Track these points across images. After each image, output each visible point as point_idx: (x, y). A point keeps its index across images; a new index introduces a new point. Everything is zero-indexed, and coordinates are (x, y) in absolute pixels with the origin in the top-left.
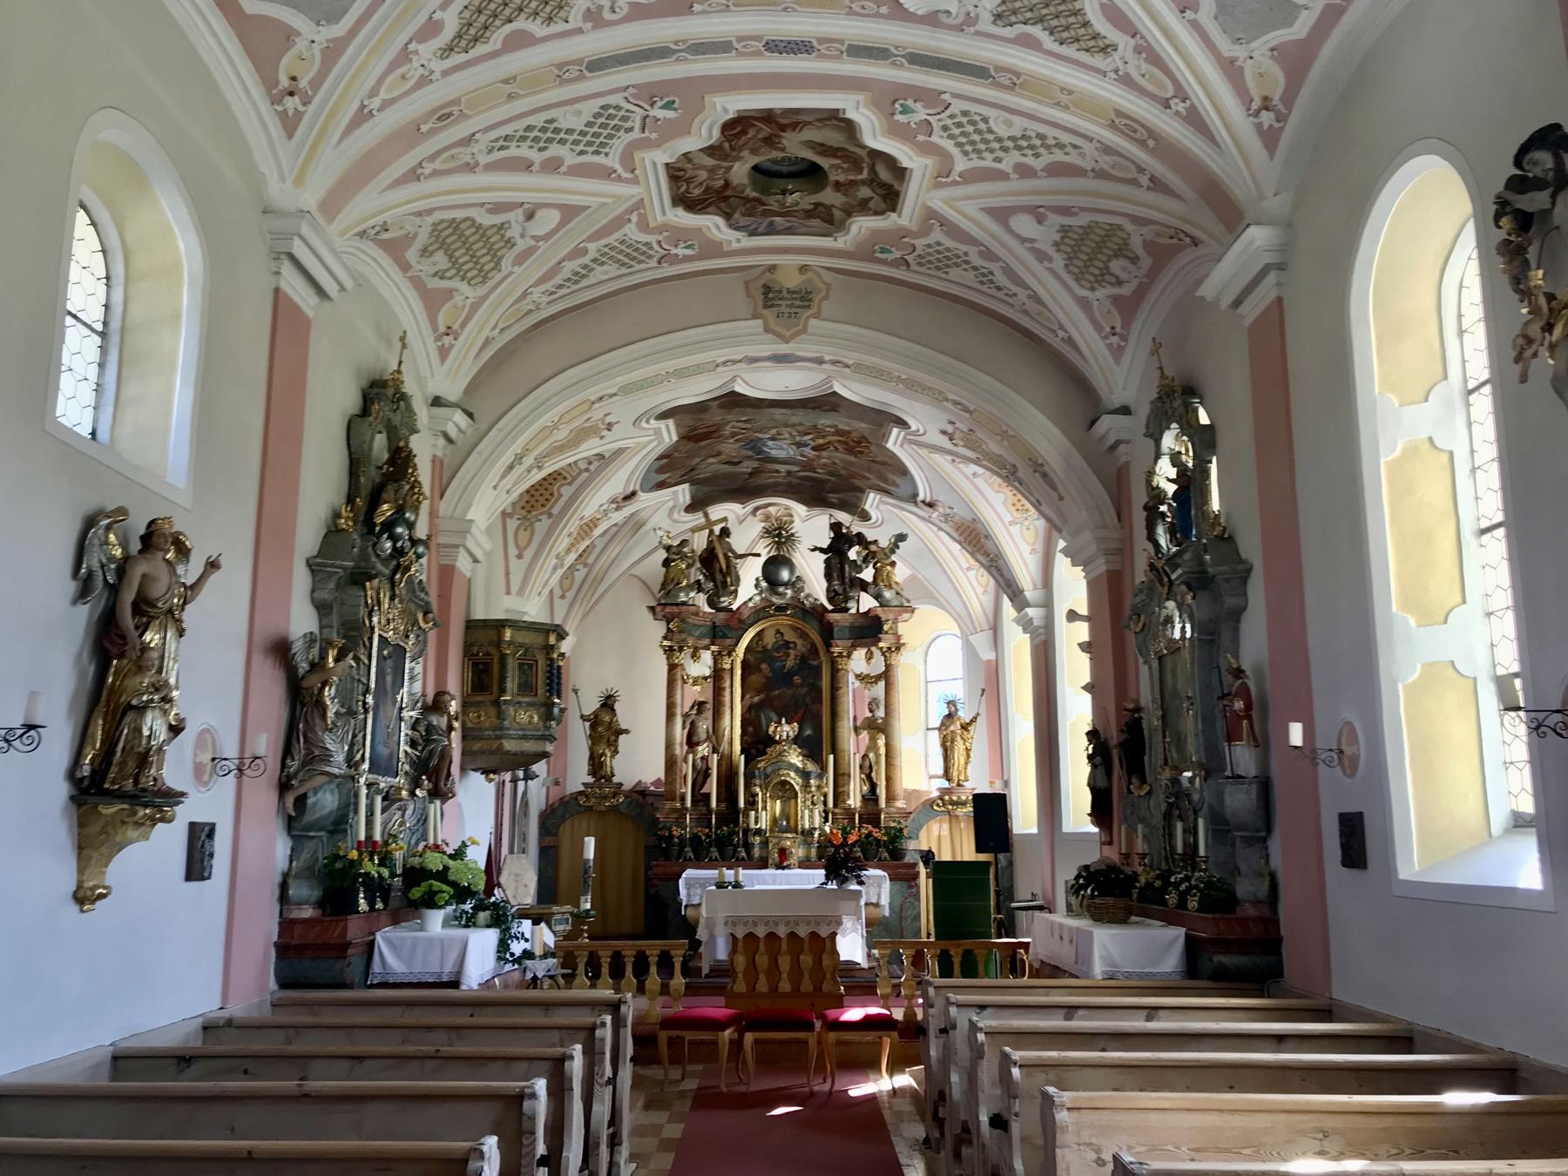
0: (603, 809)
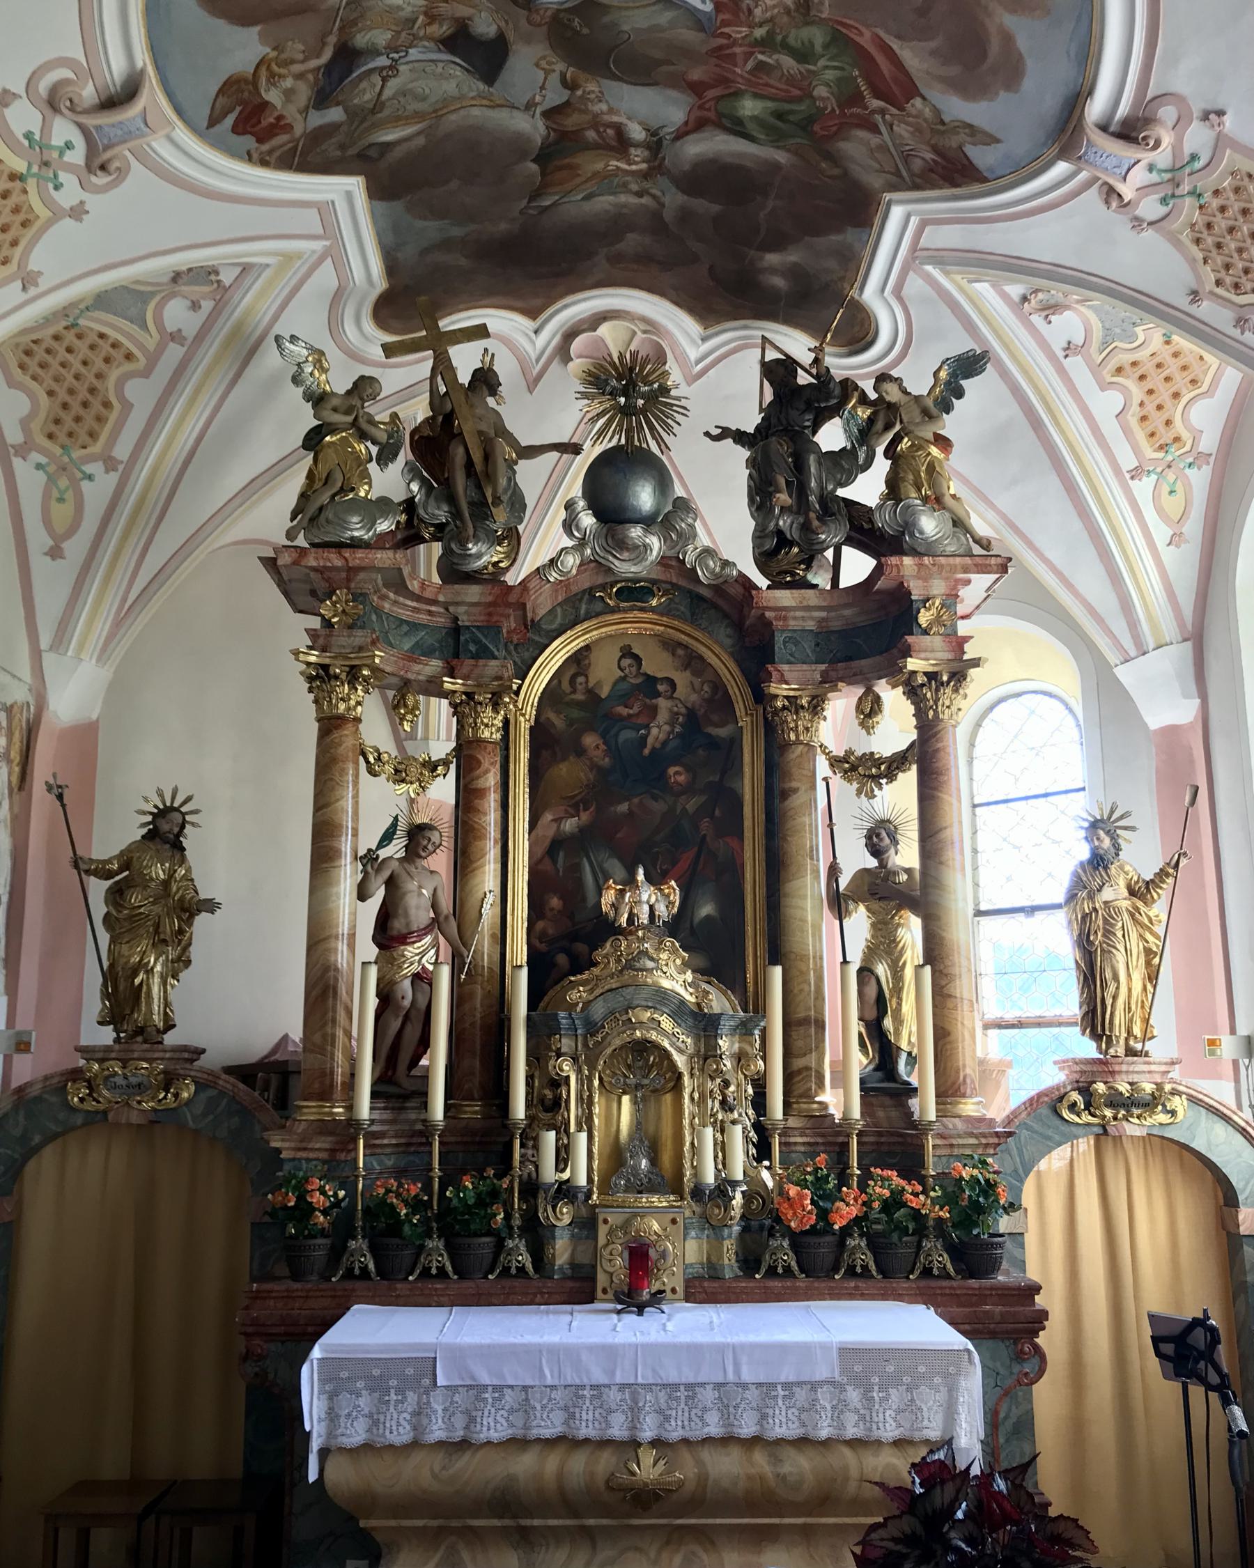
0: (135, 1118)
